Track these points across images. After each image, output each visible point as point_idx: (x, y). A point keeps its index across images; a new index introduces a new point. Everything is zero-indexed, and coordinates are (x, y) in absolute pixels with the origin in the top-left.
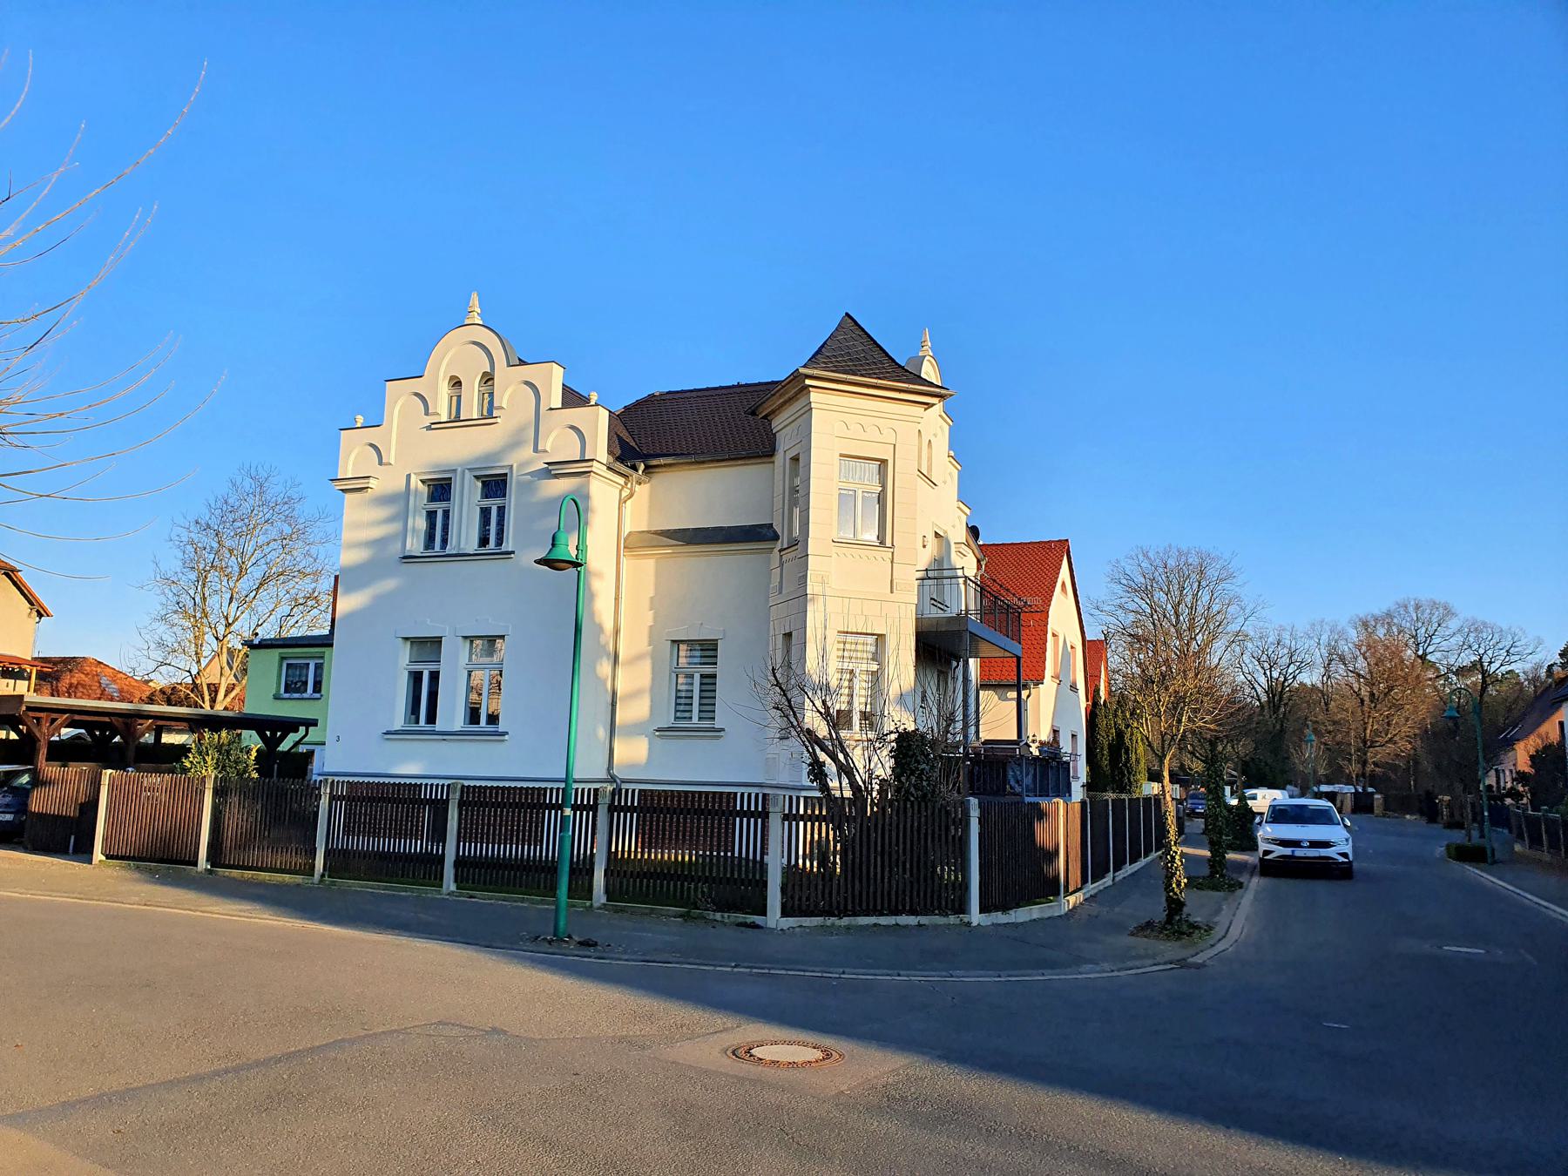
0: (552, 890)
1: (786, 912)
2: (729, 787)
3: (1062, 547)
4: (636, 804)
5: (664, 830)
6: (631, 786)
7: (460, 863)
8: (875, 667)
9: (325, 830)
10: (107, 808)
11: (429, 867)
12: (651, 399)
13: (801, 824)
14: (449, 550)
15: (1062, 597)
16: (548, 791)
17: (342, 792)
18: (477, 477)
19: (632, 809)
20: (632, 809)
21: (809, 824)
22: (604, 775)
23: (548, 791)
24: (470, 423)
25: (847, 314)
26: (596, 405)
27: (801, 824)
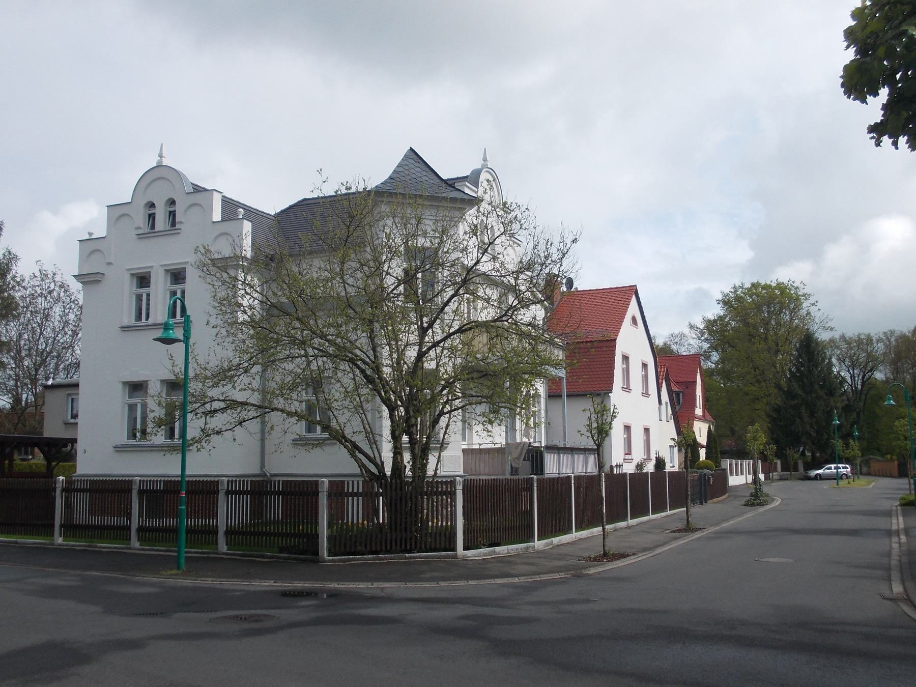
0: (176, 541)
1: (330, 553)
2: (299, 477)
3: (633, 291)
4: (281, 490)
5: (295, 505)
6: (278, 479)
7: (140, 529)
8: (844, 339)
9: (225, 521)
10: (139, 513)
11: (122, 532)
12: (304, 204)
13: (350, 498)
14: (151, 321)
15: (633, 328)
16: (277, 482)
17: (160, 487)
18: (167, 271)
19: (278, 493)
20: (278, 493)
21: (355, 498)
22: (258, 472)
23: (277, 482)
24: (163, 234)
25: (411, 149)
26: (243, 218)
27: (350, 498)
